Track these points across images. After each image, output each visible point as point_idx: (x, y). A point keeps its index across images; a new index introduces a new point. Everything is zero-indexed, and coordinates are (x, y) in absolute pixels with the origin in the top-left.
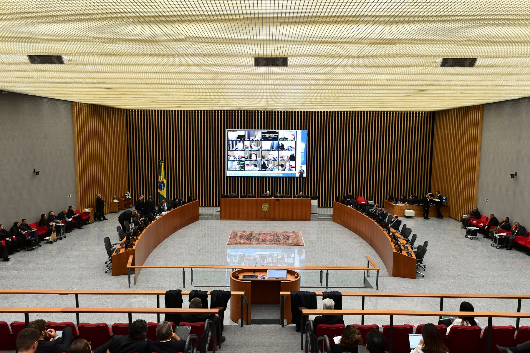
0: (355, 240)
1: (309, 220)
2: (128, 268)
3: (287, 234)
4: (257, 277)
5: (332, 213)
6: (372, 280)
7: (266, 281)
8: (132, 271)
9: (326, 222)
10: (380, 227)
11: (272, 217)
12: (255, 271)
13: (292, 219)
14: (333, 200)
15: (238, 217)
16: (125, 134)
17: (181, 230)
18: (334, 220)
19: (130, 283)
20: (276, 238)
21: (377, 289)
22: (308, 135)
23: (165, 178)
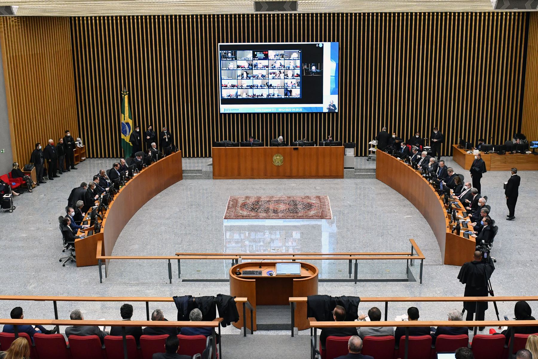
0: (405, 209)
1: (342, 177)
2: (98, 259)
3: (309, 201)
4: (260, 273)
5: (375, 167)
6: (415, 271)
7: (274, 278)
8: (103, 261)
11: (321, 173)
12: (261, 265)
13: (317, 176)
15: (238, 175)
16: (71, 53)
17: (158, 196)
18: (378, 177)
19: (101, 277)
20: (292, 208)
21: (421, 283)
23: (130, 117)
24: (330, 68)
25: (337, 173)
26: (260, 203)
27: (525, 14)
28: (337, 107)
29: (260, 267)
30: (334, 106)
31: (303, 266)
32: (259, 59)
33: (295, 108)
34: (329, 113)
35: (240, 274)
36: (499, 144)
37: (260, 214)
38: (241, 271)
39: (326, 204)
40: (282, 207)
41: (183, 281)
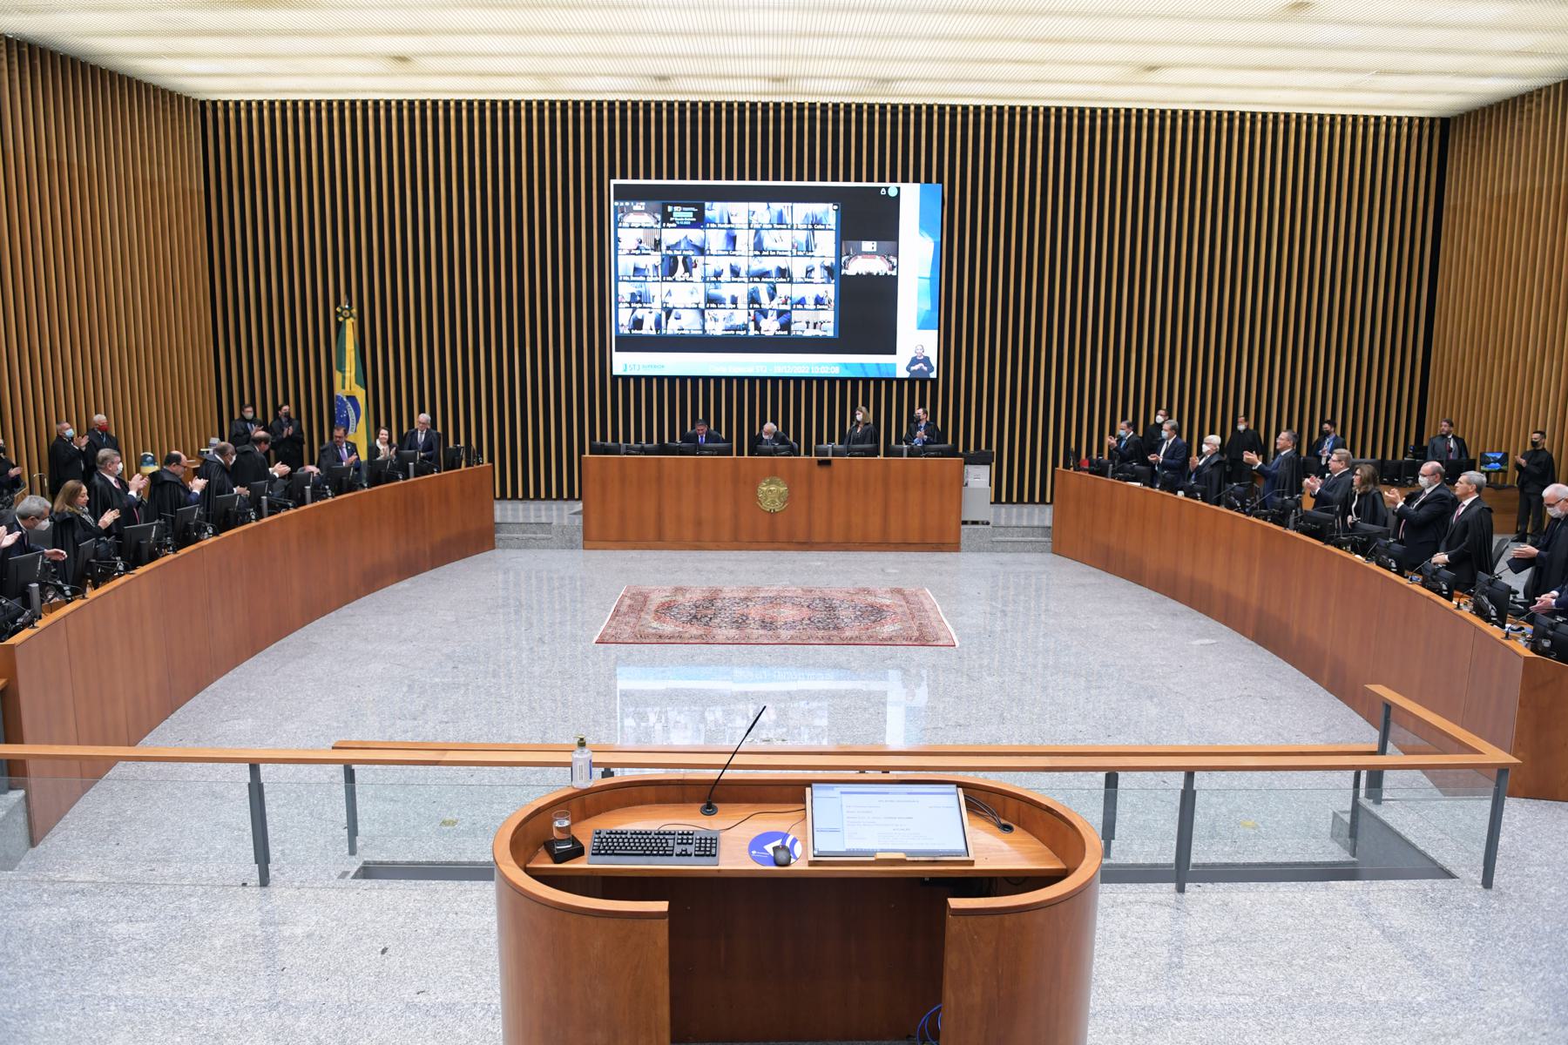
1: (955, 547)
3: (870, 599)
4: (708, 847)
5: (1048, 523)
9: (1027, 557)
10: (1329, 547)
12: (713, 795)
13: (884, 544)
14: (1055, 464)
15: (653, 535)
18: (1059, 549)
20: (819, 615)
22: (948, 203)
23: (362, 380)
24: (915, 260)
25: (940, 536)
26: (719, 604)
27: (1438, 123)
28: (934, 364)
29: (709, 809)
30: (926, 360)
31: (983, 803)
32: (680, 226)
33: (819, 365)
34: (911, 381)
35: (578, 852)
36: (1390, 457)
37: (716, 631)
38: (586, 833)
39: (928, 607)
40: (788, 613)
41: (368, 871)
